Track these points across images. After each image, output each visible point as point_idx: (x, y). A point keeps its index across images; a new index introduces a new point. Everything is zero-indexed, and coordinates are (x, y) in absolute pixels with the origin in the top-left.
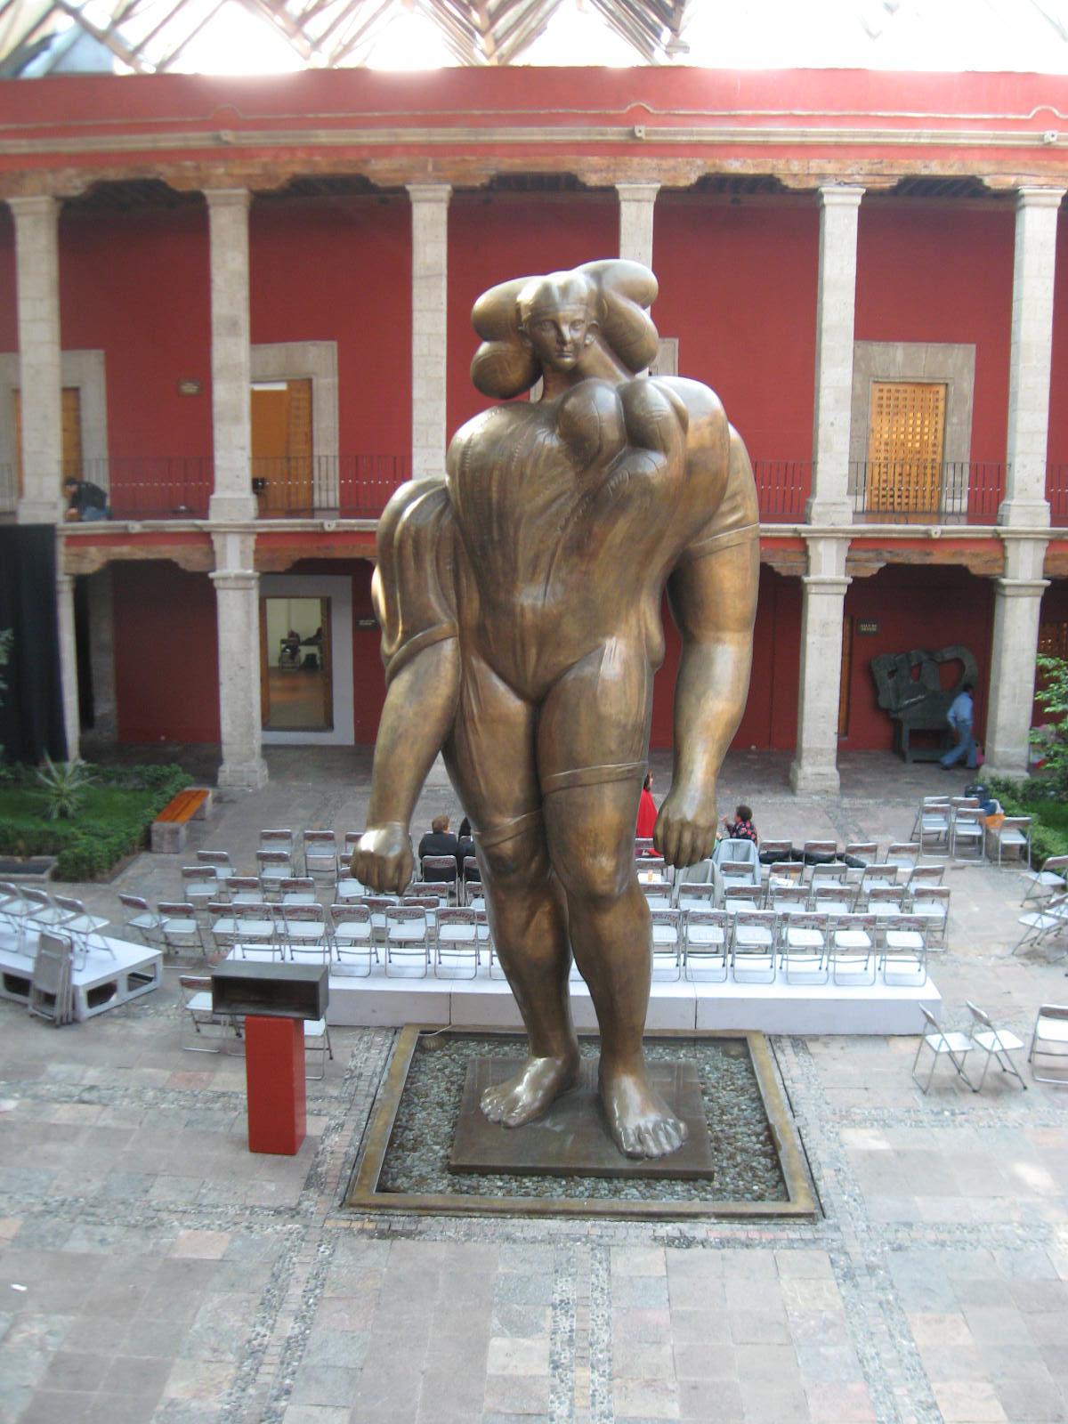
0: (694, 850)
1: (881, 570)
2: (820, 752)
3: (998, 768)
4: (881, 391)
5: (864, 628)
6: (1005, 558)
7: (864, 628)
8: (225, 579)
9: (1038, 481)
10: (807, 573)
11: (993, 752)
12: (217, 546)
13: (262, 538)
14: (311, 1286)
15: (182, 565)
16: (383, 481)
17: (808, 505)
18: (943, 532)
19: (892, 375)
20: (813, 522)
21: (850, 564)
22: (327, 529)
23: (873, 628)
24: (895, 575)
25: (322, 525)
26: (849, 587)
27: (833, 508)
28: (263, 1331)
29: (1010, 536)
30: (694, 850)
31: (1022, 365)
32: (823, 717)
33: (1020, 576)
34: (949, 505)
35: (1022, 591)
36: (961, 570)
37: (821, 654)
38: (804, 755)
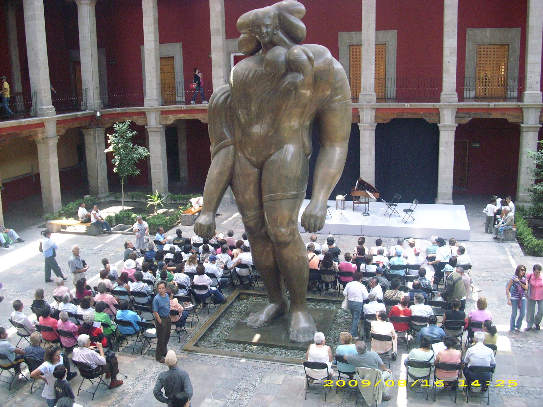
0: (315, 226)
1: (470, 121)
2: (445, 194)
3: (520, 202)
4: (480, 48)
5: (474, 145)
6: (523, 115)
7: (474, 145)
8: (444, 126)
9: (537, 83)
10: (439, 122)
11: (518, 196)
12: (524, 113)
13: (378, 110)
14: (154, 375)
15: (202, 121)
16: (189, 92)
17: (439, 95)
18: (495, 105)
19: (485, 42)
20: (441, 102)
21: (458, 119)
22: (491, 107)
23: (478, 145)
24: (475, 122)
25: (181, 107)
26: (457, 128)
27: (450, 96)
28: (130, 387)
29: (524, 106)
30: (315, 226)
31: (529, 35)
32: (446, 180)
33: (529, 123)
34: (178, 99)
35: (530, 129)
36: (504, 121)
37: (445, 155)
38: (439, 195)
